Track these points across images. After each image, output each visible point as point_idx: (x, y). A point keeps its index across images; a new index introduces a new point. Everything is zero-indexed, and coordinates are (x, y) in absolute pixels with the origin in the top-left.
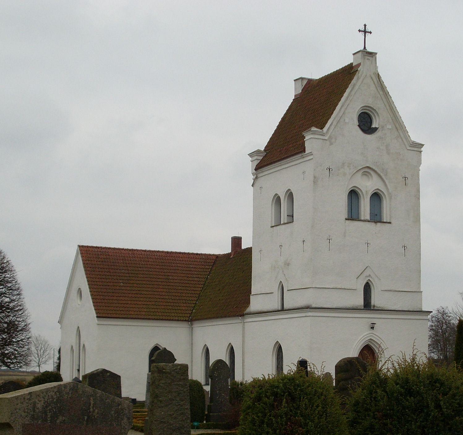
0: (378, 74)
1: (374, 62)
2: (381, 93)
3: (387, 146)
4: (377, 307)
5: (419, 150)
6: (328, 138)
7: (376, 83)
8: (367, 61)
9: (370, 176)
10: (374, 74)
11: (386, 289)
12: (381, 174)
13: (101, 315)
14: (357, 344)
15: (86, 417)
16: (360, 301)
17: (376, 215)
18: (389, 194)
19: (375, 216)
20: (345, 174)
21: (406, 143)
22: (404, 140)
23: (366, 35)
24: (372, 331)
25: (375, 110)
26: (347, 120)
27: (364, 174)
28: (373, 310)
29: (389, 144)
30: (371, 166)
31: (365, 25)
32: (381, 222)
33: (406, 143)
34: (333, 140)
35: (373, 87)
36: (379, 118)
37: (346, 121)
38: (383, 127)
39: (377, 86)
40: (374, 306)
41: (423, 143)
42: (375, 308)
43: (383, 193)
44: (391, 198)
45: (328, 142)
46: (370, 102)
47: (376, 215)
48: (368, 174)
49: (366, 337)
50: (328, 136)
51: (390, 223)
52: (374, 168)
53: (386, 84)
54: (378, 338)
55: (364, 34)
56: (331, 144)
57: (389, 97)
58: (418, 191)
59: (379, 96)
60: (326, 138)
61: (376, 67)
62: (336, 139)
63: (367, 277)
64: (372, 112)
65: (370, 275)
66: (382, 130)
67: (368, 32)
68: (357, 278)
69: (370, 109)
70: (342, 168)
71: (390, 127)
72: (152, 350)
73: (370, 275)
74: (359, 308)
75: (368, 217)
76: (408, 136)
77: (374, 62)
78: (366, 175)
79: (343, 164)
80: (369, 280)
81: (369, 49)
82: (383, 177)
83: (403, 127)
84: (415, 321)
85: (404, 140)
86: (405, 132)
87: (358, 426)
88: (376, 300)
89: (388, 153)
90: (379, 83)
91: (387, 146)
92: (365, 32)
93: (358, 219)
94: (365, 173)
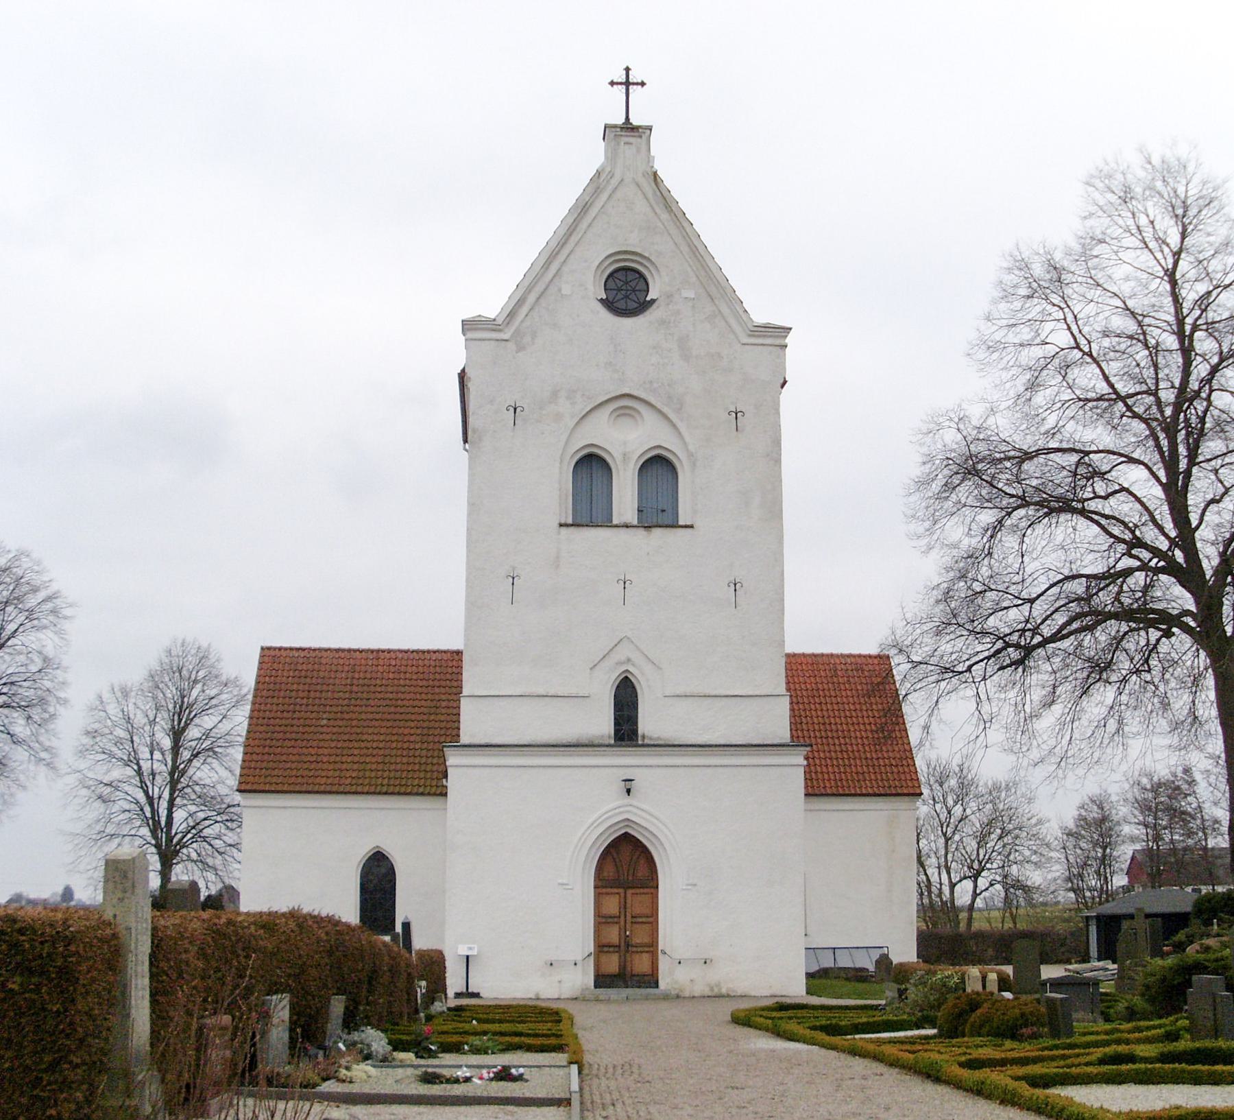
0: (655, 174)
1: (644, 147)
2: (665, 216)
3: (683, 343)
4: (651, 739)
5: (778, 342)
6: (512, 336)
7: (650, 195)
8: (627, 146)
9: (638, 418)
10: (644, 176)
11: (680, 690)
12: (665, 410)
13: (248, 787)
14: (584, 834)
15: (423, 983)
16: (603, 724)
17: (663, 511)
18: (691, 455)
19: (660, 514)
20: (558, 417)
21: (738, 329)
22: (732, 321)
23: (631, 91)
24: (628, 800)
25: (648, 259)
26: (566, 290)
27: (618, 416)
28: (643, 746)
29: (688, 336)
30: (635, 393)
31: (627, 70)
32: (675, 525)
33: (738, 329)
34: (527, 339)
35: (641, 206)
36: (660, 276)
37: (563, 292)
38: (669, 296)
39: (653, 202)
40: (643, 737)
41: (788, 326)
42: (646, 741)
43: (674, 454)
44: (694, 465)
45: (511, 346)
46: (633, 242)
47: (663, 511)
48: (627, 411)
49: (607, 819)
50: (512, 330)
51: (691, 527)
52: (643, 395)
53: (675, 194)
54: (648, 817)
55: (624, 91)
56: (521, 348)
57: (686, 224)
58: (777, 442)
59: (659, 224)
60: (506, 336)
61: (649, 159)
62: (534, 335)
63: (620, 663)
64: (641, 264)
65: (629, 660)
66: (668, 304)
67: (637, 84)
68: (591, 669)
69: (638, 258)
70: (550, 403)
71: (690, 294)
72: (370, 858)
73: (629, 660)
74: (596, 742)
75: (631, 516)
76: (741, 312)
77: (644, 147)
78: (629, 415)
79: (555, 394)
80: (627, 671)
81: (635, 121)
82: (672, 416)
83: (729, 291)
84: (488, 770)
85: (732, 321)
86: (734, 302)
87: (920, 1014)
88: (648, 724)
89: (686, 357)
90: (658, 193)
91: (683, 343)
92: (627, 84)
93: (606, 522)
94: (622, 412)
